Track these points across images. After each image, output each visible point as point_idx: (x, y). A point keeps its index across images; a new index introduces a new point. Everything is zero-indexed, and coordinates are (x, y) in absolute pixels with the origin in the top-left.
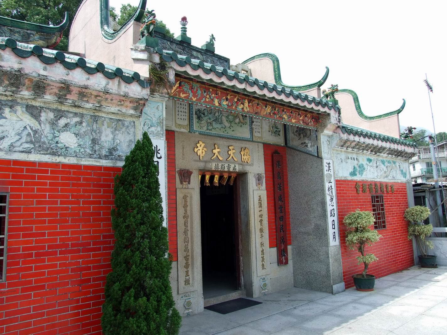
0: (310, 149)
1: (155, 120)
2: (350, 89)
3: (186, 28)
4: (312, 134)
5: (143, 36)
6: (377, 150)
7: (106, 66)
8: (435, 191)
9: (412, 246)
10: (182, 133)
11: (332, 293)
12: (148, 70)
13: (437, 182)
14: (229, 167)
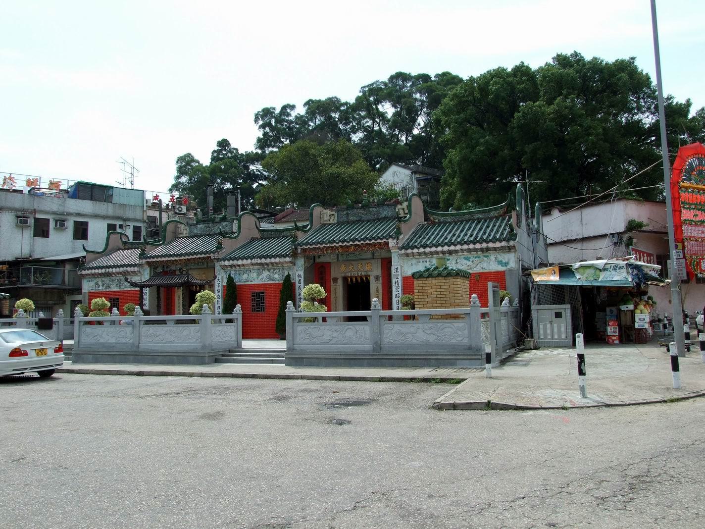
1: (300, 265)
10: (334, 262)
14: (358, 274)
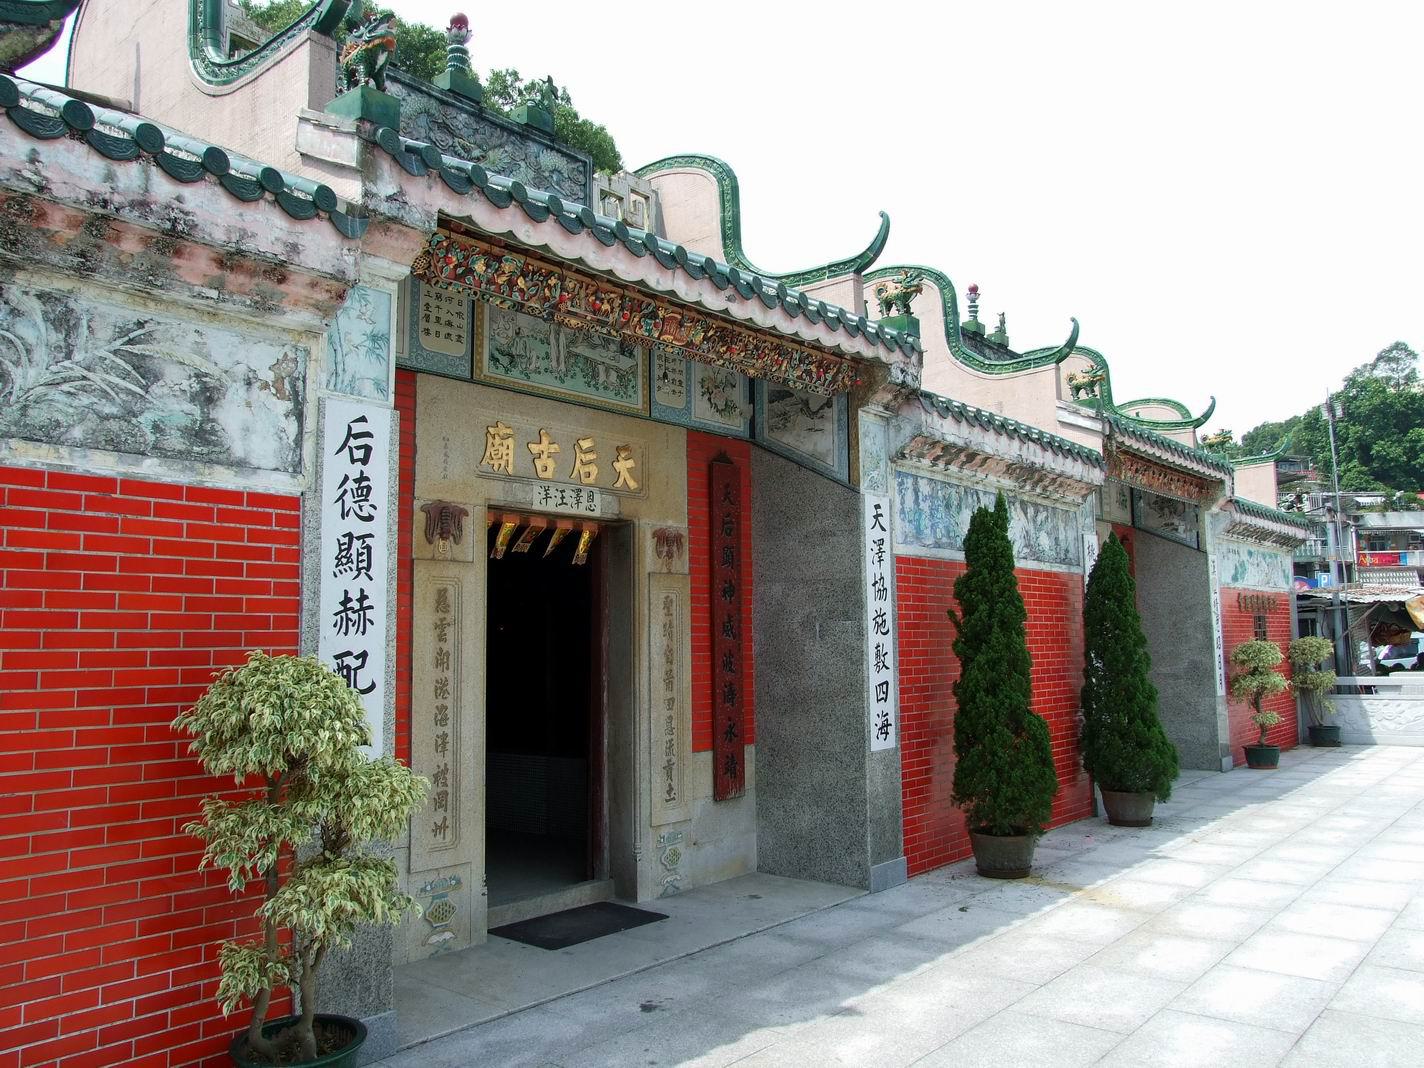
0: (1184, 536)
2: (1176, 400)
3: (465, 52)
4: (1187, 510)
5: (352, 82)
6: (1262, 535)
7: (286, 178)
8: (1333, 610)
9: (1295, 709)
11: (1221, 771)
12: (109, 96)
13: (1336, 594)
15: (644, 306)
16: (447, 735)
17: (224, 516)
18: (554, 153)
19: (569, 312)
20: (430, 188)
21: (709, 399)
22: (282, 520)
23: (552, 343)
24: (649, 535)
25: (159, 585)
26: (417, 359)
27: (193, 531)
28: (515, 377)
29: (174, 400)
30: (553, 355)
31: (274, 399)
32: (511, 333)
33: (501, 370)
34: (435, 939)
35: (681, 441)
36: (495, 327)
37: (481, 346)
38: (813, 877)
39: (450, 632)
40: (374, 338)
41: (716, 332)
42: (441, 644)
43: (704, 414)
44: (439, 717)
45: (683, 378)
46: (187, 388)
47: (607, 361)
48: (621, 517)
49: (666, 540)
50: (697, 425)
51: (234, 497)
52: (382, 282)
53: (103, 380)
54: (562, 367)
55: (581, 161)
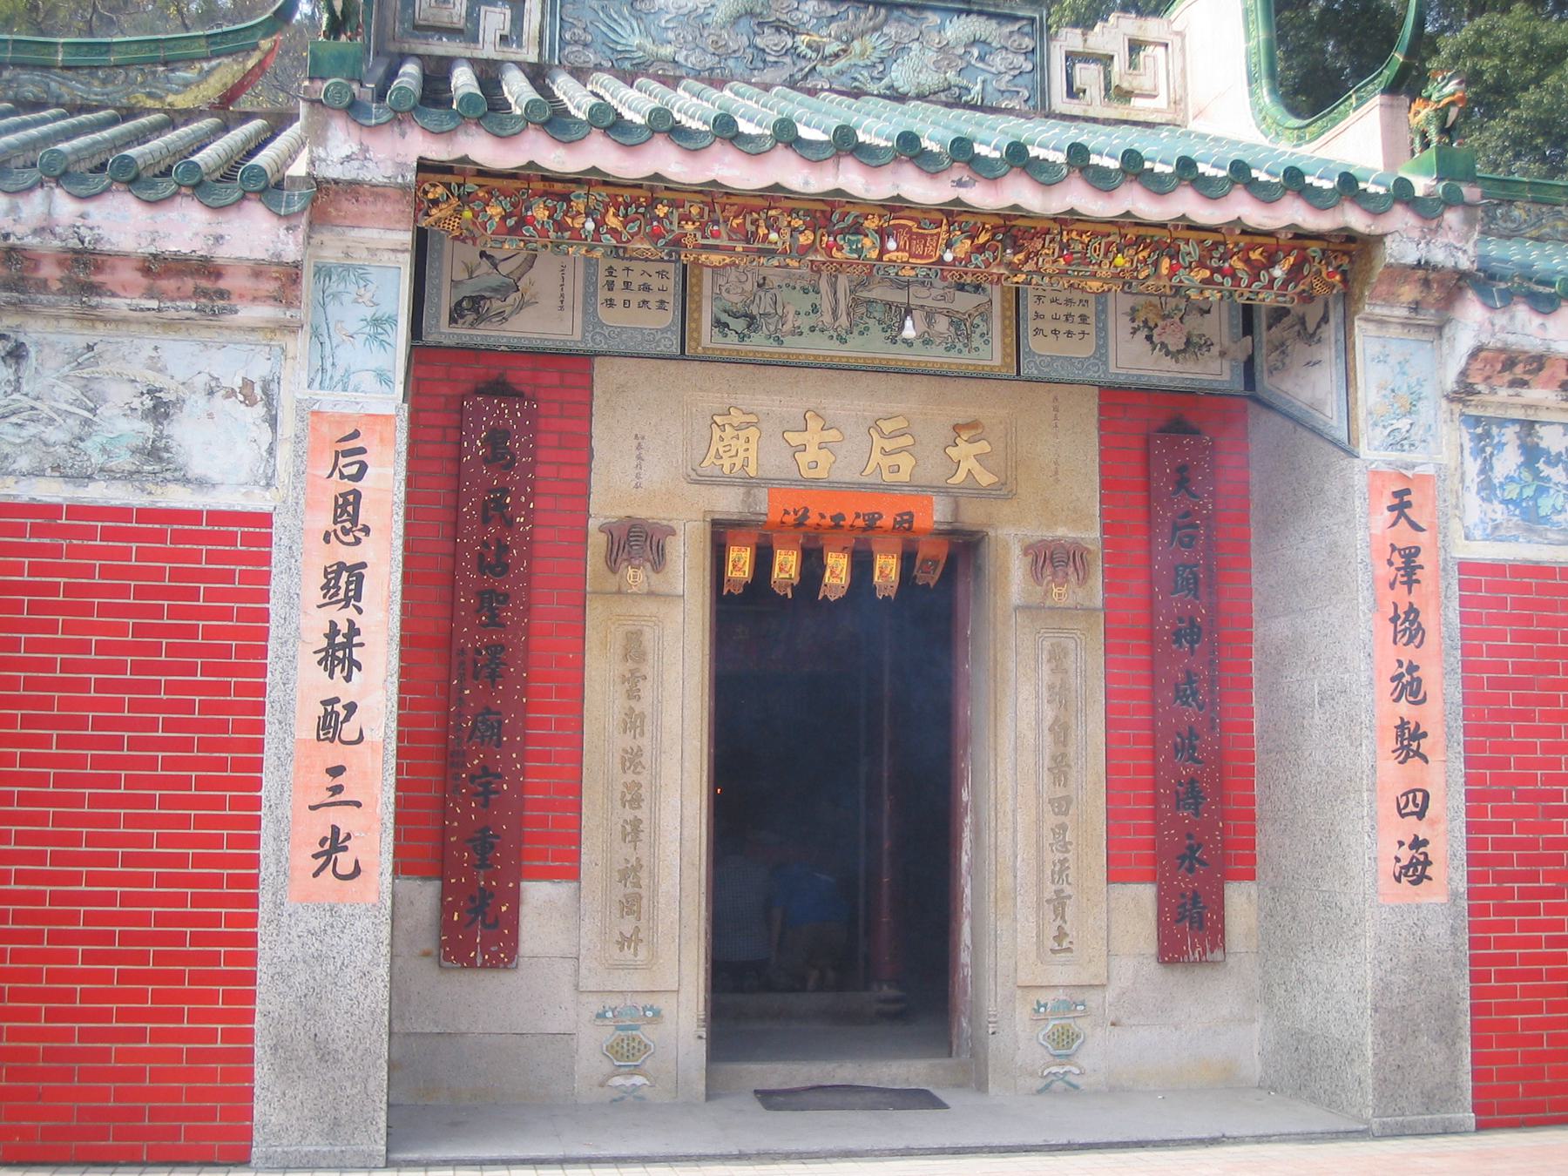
15: (835, 218)
16: (641, 821)
17: (178, 537)
18: (973, 17)
19: (704, 247)
20: (403, 135)
21: (1149, 338)
22: (248, 539)
23: (823, 291)
24: (1016, 551)
25: (105, 610)
26: (593, 340)
27: (142, 554)
28: (759, 344)
29: (125, 420)
30: (826, 306)
31: (243, 407)
32: (748, 286)
33: (733, 337)
34: (617, 1081)
35: (1087, 409)
36: (721, 281)
37: (699, 309)
38: (1313, 1099)
39: (646, 690)
40: (376, 322)
41: (994, 235)
42: (633, 703)
43: (1134, 360)
44: (628, 797)
45: (1090, 311)
46: (138, 406)
47: (929, 303)
48: (958, 525)
49: (1051, 559)
50: (1122, 379)
51: (193, 516)
52: (386, 256)
53: (51, 408)
54: (844, 321)
55: (1023, 18)
